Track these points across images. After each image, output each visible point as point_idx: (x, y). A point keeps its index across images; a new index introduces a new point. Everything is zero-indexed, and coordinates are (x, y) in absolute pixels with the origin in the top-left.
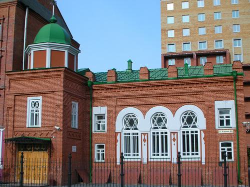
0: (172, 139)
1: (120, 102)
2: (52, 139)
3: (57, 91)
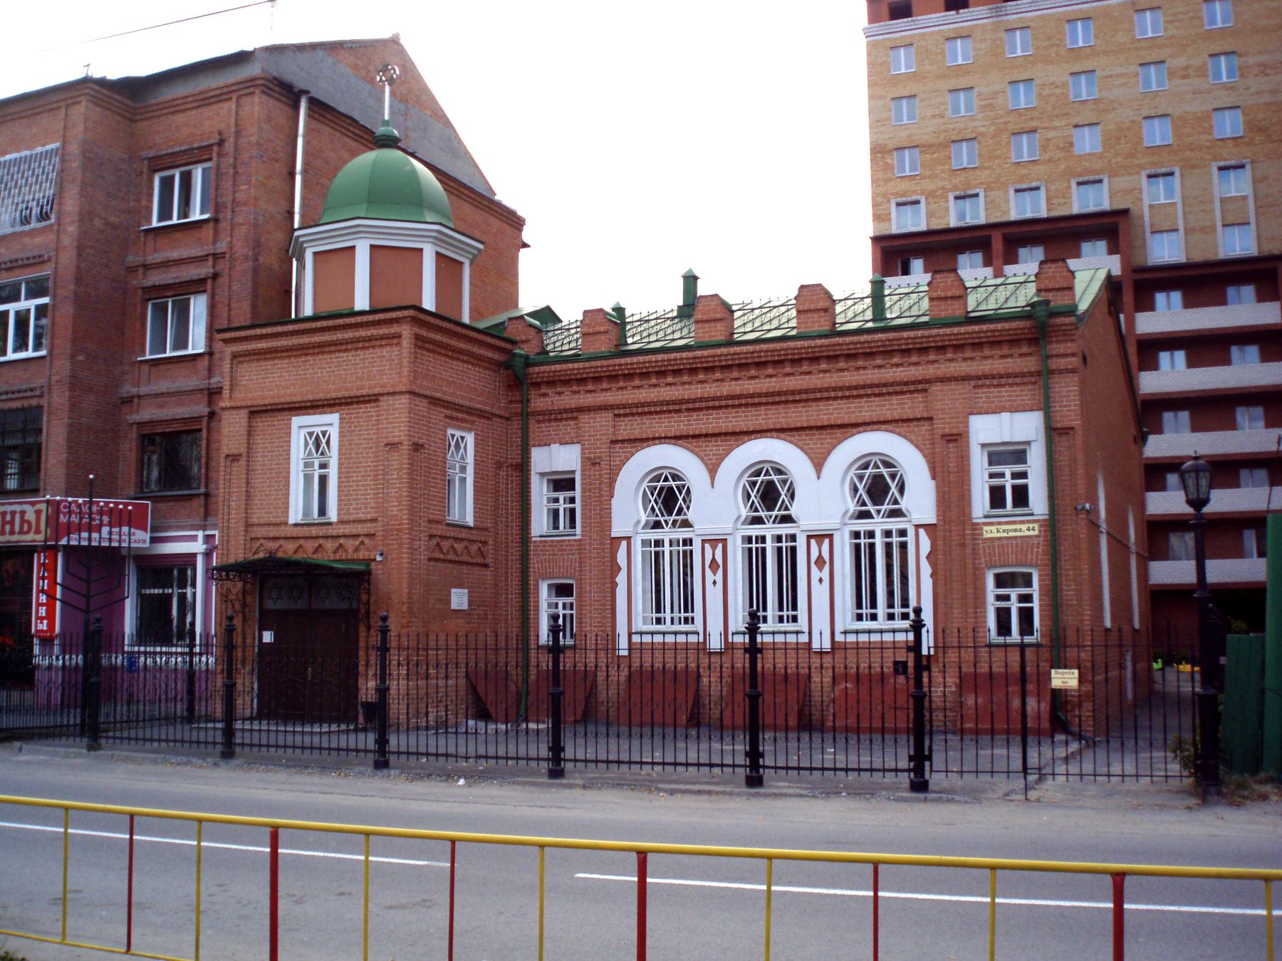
0: (813, 559)
1: (629, 428)
3: (389, 394)
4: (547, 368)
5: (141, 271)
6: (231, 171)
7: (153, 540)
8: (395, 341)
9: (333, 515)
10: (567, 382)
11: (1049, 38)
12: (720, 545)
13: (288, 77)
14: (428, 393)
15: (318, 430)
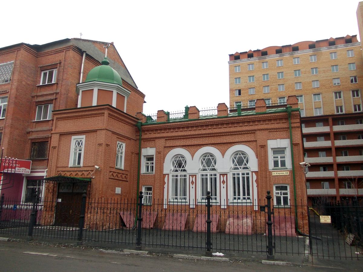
0: (221, 181)
1: (169, 143)
2: (92, 180)
3: (100, 130)
4: (147, 126)
5: (36, 97)
6: (62, 71)
7: (31, 172)
8: (103, 115)
9: (81, 165)
10: (152, 130)
11: (272, 64)
12: (194, 177)
13: (80, 48)
14: (112, 130)
15: (79, 140)
